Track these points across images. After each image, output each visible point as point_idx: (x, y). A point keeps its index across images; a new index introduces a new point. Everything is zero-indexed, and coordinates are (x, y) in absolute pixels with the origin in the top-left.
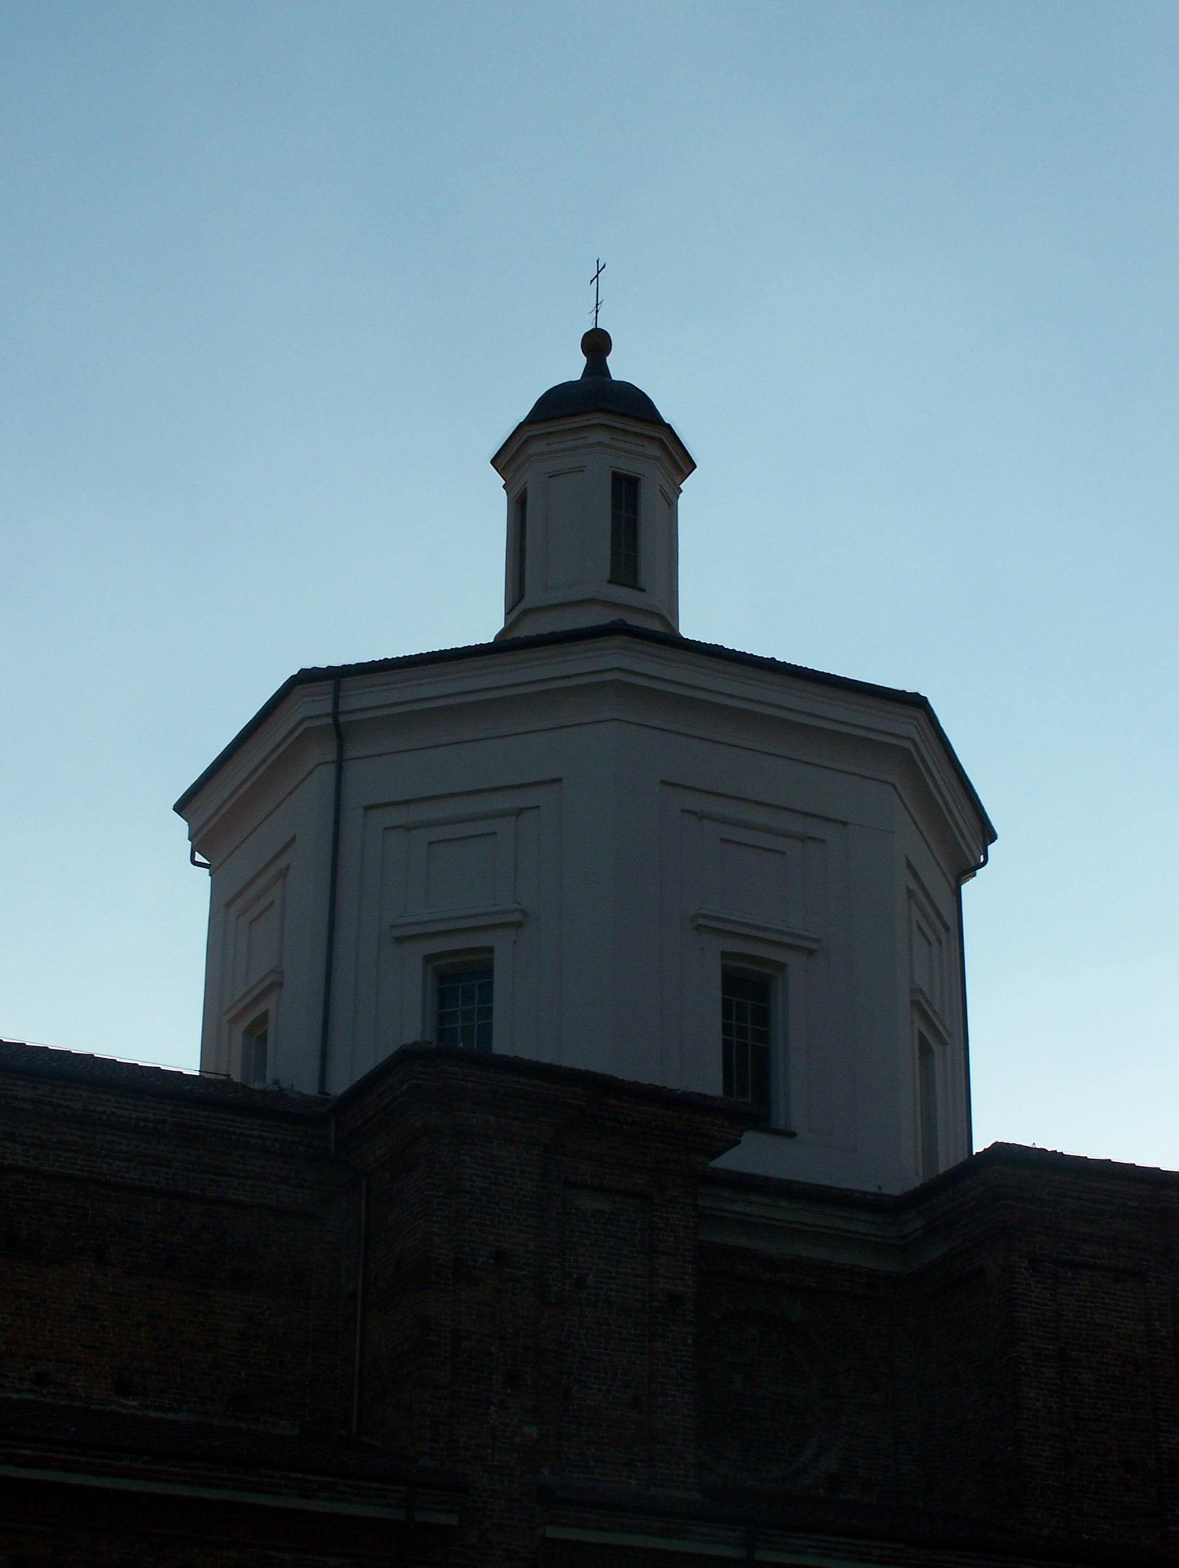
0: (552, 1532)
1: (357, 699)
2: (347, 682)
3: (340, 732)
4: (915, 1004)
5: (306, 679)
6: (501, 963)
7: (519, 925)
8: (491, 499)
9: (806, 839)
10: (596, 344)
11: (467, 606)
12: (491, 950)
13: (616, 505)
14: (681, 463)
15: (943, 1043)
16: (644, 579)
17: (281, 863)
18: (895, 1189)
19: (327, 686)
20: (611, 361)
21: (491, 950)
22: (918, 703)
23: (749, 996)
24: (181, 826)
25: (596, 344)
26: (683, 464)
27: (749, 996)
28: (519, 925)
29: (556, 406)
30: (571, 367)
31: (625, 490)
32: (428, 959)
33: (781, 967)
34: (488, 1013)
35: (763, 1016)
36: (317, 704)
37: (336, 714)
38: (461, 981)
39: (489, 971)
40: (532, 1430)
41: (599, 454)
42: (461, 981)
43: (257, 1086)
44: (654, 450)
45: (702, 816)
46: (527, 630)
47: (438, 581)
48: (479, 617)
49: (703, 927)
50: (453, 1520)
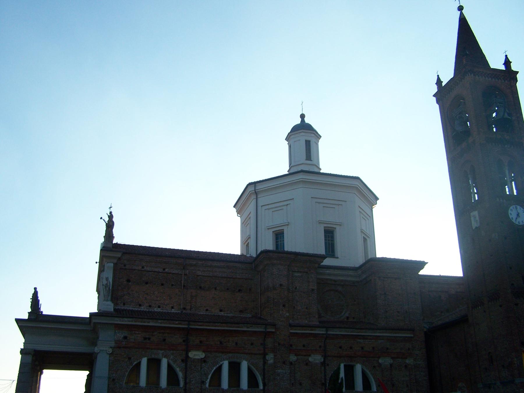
0: (291, 331)
1: (259, 187)
2: (257, 184)
3: (256, 193)
4: (361, 232)
5: (250, 184)
6: (285, 232)
7: (288, 225)
8: (285, 146)
9: (338, 205)
10: (302, 116)
11: (281, 167)
12: (283, 230)
13: (306, 146)
14: (318, 137)
15: (368, 237)
16: (312, 159)
17: (288, 202)
18: (357, 266)
19: (253, 185)
20: (305, 119)
21: (283, 230)
22: (357, 178)
23: (329, 234)
24: (235, 210)
25: (302, 116)
26: (319, 137)
27: (329, 234)
28: (288, 225)
29: (295, 129)
30: (298, 121)
31: (308, 143)
32: (273, 232)
33: (335, 228)
34: (283, 241)
35: (332, 237)
36: (252, 189)
37: (255, 190)
38: (279, 236)
39: (283, 233)
40: (288, 314)
41: (303, 137)
42: (279, 236)
43: (248, 255)
44: (313, 135)
45: (319, 203)
46: (291, 171)
47: (275, 162)
48: (284, 169)
49: (320, 223)
50: (274, 330)
